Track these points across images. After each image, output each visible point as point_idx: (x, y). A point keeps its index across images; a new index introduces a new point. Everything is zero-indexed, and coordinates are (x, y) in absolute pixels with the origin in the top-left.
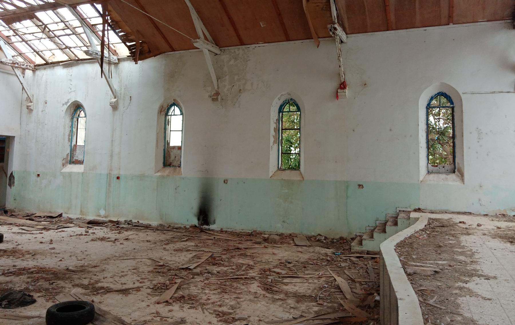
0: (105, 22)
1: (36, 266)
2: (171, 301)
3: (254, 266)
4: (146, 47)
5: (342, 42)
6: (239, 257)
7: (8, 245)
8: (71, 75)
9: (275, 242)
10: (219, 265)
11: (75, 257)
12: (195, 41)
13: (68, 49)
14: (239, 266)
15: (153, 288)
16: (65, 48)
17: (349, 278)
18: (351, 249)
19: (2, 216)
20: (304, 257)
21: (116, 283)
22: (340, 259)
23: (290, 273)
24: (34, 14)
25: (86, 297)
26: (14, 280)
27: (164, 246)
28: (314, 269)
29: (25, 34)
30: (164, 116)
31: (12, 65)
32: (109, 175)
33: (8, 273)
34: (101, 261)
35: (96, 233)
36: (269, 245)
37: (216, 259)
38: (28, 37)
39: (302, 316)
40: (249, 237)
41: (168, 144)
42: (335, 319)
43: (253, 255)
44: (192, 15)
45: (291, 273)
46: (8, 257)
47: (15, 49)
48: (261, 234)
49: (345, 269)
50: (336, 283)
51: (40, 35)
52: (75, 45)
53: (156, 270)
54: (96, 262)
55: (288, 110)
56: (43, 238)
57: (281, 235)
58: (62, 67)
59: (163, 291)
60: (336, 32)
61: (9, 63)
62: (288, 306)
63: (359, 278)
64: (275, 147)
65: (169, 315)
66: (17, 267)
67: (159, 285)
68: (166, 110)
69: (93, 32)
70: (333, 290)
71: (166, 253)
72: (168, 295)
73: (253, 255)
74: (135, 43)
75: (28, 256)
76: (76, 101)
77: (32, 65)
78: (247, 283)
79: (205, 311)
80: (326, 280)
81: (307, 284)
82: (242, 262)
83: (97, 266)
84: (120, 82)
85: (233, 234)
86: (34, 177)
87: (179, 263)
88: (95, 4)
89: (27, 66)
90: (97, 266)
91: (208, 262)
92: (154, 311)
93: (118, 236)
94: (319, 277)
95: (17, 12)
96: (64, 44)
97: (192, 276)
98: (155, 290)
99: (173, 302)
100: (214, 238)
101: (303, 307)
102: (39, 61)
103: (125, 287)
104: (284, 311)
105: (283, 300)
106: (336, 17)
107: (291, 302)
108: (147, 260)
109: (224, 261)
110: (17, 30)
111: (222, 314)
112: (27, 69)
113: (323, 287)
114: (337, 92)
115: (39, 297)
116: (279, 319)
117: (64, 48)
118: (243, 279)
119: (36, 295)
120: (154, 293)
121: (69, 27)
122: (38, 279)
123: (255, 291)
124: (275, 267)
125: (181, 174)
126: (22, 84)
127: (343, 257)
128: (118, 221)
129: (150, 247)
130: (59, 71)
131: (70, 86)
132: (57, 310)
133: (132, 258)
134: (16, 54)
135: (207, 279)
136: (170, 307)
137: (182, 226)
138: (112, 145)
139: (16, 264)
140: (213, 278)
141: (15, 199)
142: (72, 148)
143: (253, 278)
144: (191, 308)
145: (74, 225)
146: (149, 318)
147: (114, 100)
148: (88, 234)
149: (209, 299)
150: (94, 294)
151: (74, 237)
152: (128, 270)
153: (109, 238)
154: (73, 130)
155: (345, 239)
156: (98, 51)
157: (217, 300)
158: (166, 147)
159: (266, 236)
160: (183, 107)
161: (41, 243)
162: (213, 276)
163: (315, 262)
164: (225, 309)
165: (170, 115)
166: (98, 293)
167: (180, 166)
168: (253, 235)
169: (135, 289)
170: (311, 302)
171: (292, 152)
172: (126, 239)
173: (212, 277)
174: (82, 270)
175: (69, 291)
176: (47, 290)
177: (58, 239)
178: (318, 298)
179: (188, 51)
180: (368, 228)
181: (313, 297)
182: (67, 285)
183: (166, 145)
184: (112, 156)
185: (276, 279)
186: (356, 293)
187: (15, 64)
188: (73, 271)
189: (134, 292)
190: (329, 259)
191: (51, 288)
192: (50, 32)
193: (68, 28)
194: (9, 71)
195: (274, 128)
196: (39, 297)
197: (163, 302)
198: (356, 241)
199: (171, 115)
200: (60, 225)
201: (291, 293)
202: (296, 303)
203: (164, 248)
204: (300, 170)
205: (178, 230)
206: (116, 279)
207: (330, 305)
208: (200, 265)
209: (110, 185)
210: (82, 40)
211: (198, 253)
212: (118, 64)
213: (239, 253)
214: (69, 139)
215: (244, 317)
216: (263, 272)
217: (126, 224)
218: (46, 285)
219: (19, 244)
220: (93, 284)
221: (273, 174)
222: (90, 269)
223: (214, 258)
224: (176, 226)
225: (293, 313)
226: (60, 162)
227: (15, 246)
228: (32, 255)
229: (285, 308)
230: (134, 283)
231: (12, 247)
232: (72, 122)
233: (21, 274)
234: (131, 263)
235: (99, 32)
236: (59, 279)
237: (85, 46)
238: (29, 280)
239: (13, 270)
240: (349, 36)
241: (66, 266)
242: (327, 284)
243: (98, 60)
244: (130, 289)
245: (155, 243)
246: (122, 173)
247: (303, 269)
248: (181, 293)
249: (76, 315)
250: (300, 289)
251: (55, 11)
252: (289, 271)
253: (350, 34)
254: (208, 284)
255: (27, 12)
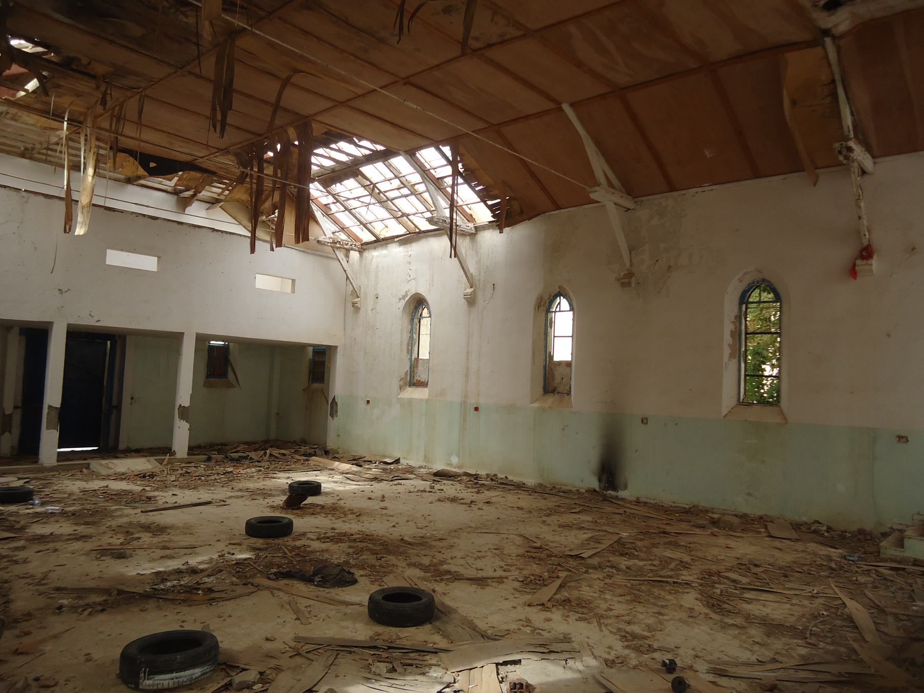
0: (456, 173)
1: (361, 531)
2: (549, 605)
3: (690, 564)
4: (516, 205)
5: (864, 172)
6: (667, 546)
7: (326, 498)
8: (410, 256)
9: (731, 527)
10: (631, 556)
11: (413, 523)
12: (593, 189)
13: (405, 218)
14: (665, 562)
15: (522, 581)
16: (402, 216)
17: (872, 605)
18: (879, 552)
19: (323, 458)
20: (785, 559)
21: (468, 567)
22: (857, 569)
23: (757, 584)
24: (358, 169)
25: (425, 583)
26: (331, 548)
27: (544, 518)
28: (803, 582)
29: (349, 199)
30: (544, 314)
31: (332, 245)
32: (464, 404)
33: (324, 538)
34: (449, 533)
35: (445, 490)
36: (719, 531)
37: (626, 547)
38: (353, 204)
39: (774, 660)
40: (686, 515)
41: (551, 357)
42: (840, 675)
43: (691, 545)
44: (588, 150)
45: (759, 584)
46: (325, 515)
47: (336, 222)
48: (707, 511)
49: (866, 587)
50: (846, 610)
51: (367, 199)
52: (414, 211)
53: (529, 554)
54: (442, 532)
55: (758, 299)
56: (372, 492)
57: (744, 517)
58: (397, 244)
59: (538, 587)
60: (851, 155)
61: (328, 243)
62: (749, 640)
63: (895, 608)
64: (733, 364)
65: (546, 626)
66: (336, 531)
67: (533, 578)
68: (547, 304)
69: (440, 189)
70: (839, 623)
71: (545, 528)
72: (546, 594)
73: (691, 545)
74: (499, 200)
75: (351, 516)
76: (417, 294)
77: (358, 244)
78: (677, 592)
79: (604, 628)
80: (826, 603)
81: (788, 606)
82: (670, 555)
83: (442, 539)
84: (479, 262)
85: (659, 508)
86: (362, 404)
87: (565, 547)
88: (440, 146)
89: (351, 245)
90: (442, 539)
91: (612, 549)
92: (523, 617)
93: (475, 497)
94: (813, 597)
95: (336, 169)
96: (400, 210)
97: (584, 570)
98: (526, 584)
99: (553, 606)
100: (625, 511)
101: (778, 644)
102: (367, 237)
103: (480, 574)
104: (741, 646)
105: (740, 628)
106: (851, 128)
107: (756, 633)
108: (516, 537)
109: (640, 550)
110: (338, 194)
111: (631, 636)
112: (352, 249)
113: (819, 614)
114: (854, 265)
115: (361, 576)
116: (732, 660)
117: (400, 216)
118: (670, 584)
119: (358, 573)
120: (524, 590)
121: (406, 184)
122: (361, 551)
123: (691, 606)
124: (729, 570)
125: (572, 407)
126: (345, 271)
127: (864, 566)
128: (476, 475)
129: (522, 518)
130: (395, 250)
131: (409, 271)
132: (384, 598)
133: (494, 531)
134: (337, 230)
135: (610, 577)
136: (548, 615)
137: (574, 489)
138: (468, 359)
139: (334, 526)
140: (619, 577)
141: (338, 436)
142: (413, 363)
143: (688, 584)
144: (580, 619)
145: (415, 476)
146: (513, 626)
147: (470, 290)
148: (433, 491)
149: (611, 610)
150: (436, 581)
151: (414, 493)
152: (486, 550)
153: (462, 499)
154: (413, 336)
155: (869, 534)
156: (447, 217)
157: (624, 612)
158: (548, 363)
159: (716, 516)
160: (574, 298)
161: (370, 499)
162: (619, 573)
163: (805, 568)
164: (636, 629)
165: (553, 312)
166: (442, 580)
167: (569, 393)
168: (692, 513)
169: (496, 580)
170: (795, 638)
171: (766, 373)
172: (488, 503)
173: (618, 575)
174: (422, 543)
175: (402, 571)
176: (373, 566)
177: (392, 495)
178: (808, 633)
179: (581, 208)
180: (916, 517)
181: (799, 629)
182: (399, 563)
183: (548, 359)
184: (468, 376)
185: (730, 590)
186: (886, 634)
187: (335, 243)
188: (410, 544)
189: (494, 584)
190: (833, 565)
191: (378, 564)
192: (381, 194)
193: (405, 186)
194: (330, 254)
195: (732, 331)
196: (361, 576)
197: (537, 605)
198: (890, 538)
199: (555, 312)
200: (397, 475)
201: (756, 617)
202: (765, 636)
203: (543, 521)
204: (780, 407)
205: (566, 495)
206: (469, 562)
207: (832, 648)
208: (598, 552)
209: (464, 420)
210: (423, 202)
211: (597, 533)
212: (475, 234)
213: (666, 540)
214: (408, 349)
215: (669, 647)
216: (706, 577)
217: (489, 479)
218: (372, 559)
219: (341, 499)
220: (435, 565)
221: (729, 412)
222: (434, 543)
223: (623, 545)
224: (564, 488)
225: (758, 653)
226: (396, 384)
227: (335, 502)
228: (357, 516)
229: (745, 642)
230: (495, 570)
231: (332, 502)
232: (412, 325)
233: (341, 541)
234: (492, 539)
235: (447, 189)
236: (389, 552)
237: (428, 210)
238: (351, 551)
239: (331, 534)
240: (878, 160)
241: (401, 535)
242: (828, 610)
243: (446, 231)
244: (489, 578)
245: (530, 512)
246: (482, 402)
247: (783, 578)
248: (565, 594)
249: (408, 609)
250: (774, 612)
251: (386, 162)
252: (755, 580)
253: (882, 156)
254: (611, 585)
255: (350, 167)
